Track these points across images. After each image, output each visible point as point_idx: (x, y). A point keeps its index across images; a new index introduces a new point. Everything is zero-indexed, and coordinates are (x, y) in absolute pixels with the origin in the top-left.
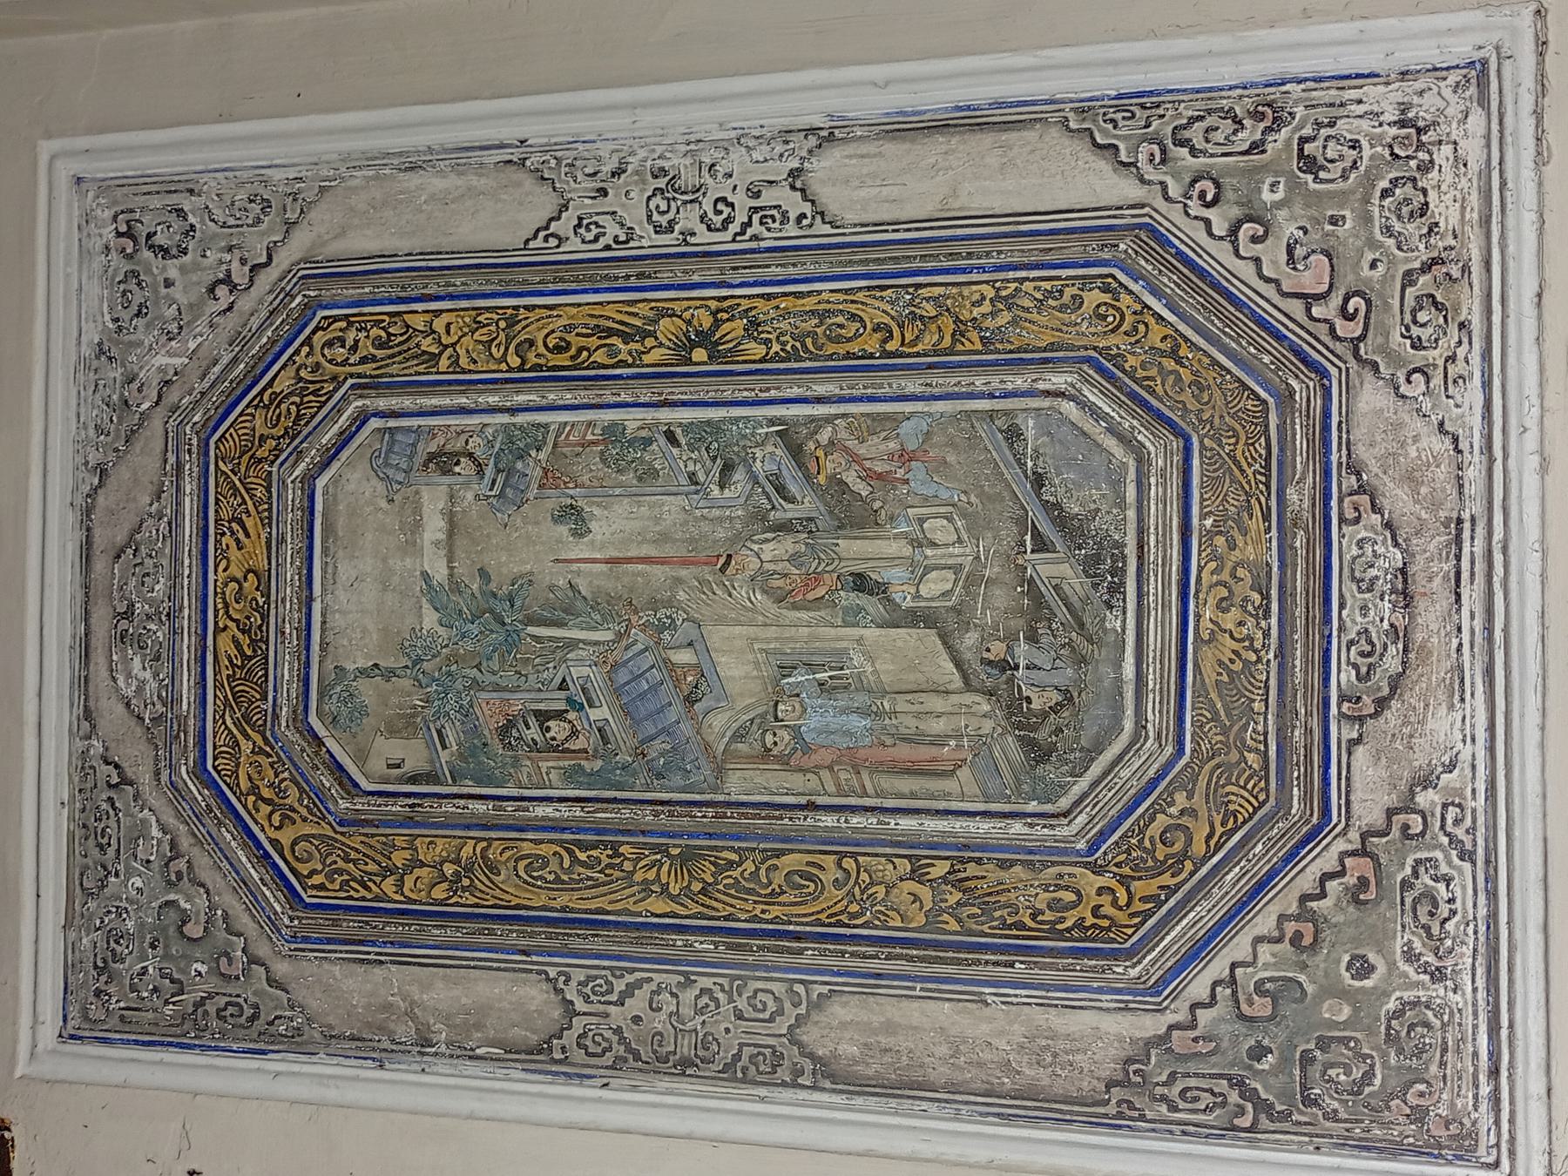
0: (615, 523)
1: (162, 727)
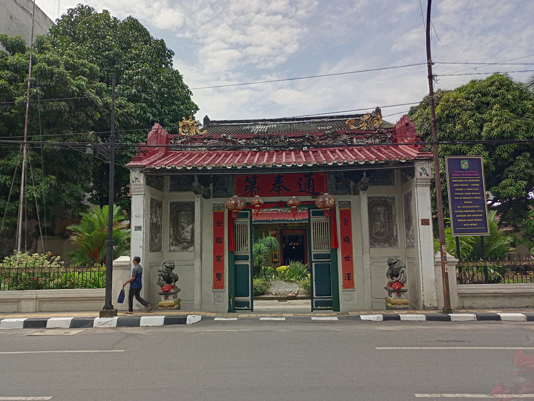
0: (383, 218)
1: (374, 201)
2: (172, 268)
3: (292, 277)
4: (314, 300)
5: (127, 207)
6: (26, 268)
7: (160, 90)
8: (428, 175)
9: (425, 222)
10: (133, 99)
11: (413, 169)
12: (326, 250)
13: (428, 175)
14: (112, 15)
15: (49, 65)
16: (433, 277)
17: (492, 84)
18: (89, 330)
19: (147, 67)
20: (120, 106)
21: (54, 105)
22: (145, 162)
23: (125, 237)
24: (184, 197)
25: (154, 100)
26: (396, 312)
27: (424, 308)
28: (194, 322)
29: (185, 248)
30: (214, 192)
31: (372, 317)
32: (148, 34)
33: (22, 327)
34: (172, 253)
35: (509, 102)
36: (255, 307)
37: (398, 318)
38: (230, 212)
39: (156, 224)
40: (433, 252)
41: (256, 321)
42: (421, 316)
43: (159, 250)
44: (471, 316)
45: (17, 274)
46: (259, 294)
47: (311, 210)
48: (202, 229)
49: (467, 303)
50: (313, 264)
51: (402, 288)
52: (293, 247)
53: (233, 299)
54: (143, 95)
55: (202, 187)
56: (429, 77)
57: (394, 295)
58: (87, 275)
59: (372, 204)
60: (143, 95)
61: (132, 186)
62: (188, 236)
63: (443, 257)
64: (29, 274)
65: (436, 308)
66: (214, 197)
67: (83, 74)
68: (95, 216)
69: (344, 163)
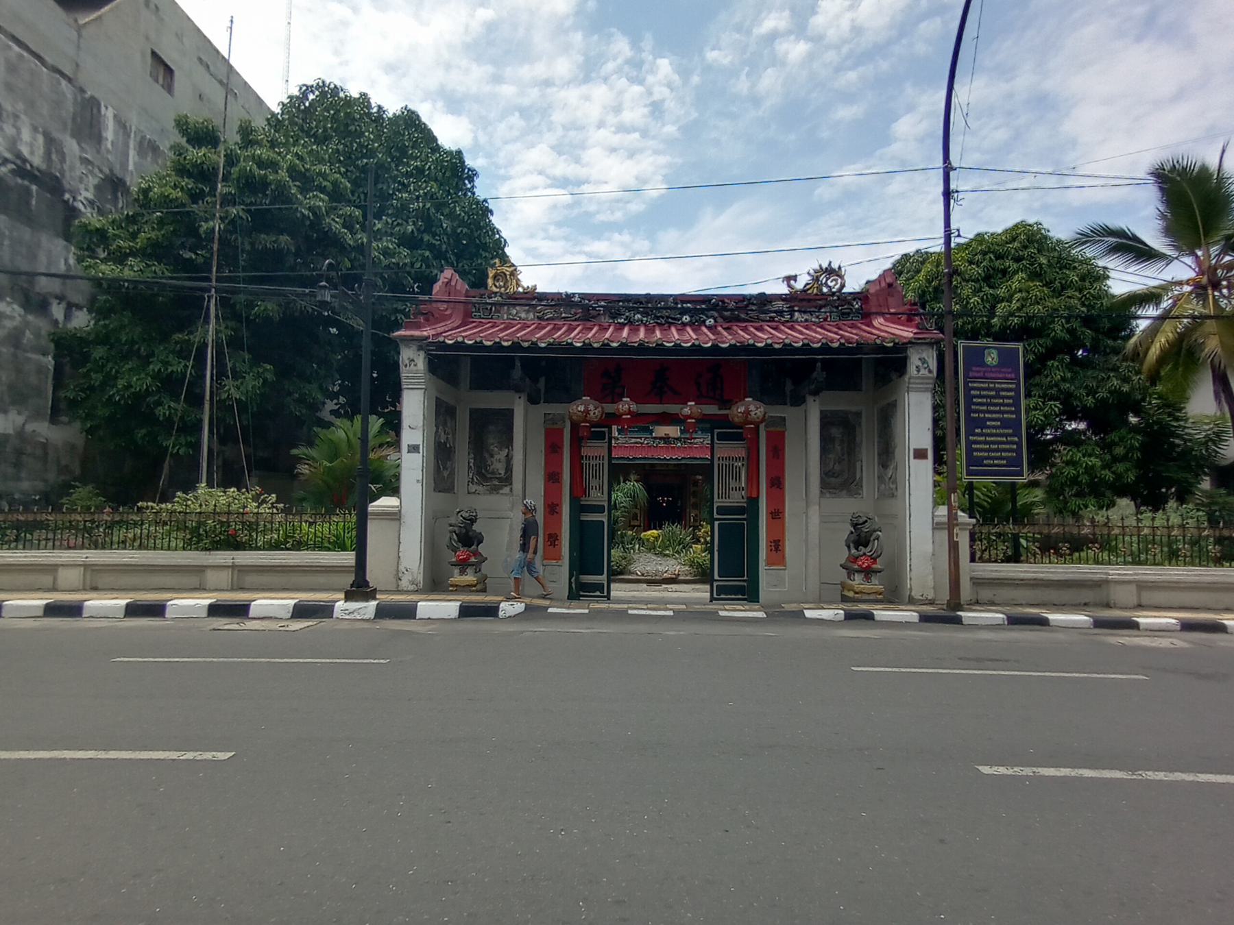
2: (473, 521)
3: (667, 548)
4: (715, 584)
5: (394, 424)
6: (215, 513)
7: (454, 229)
8: (930, 371)
9: (920, 454)
10: (411, 242)
13: (930, 371)
14: (375, 101)
15: (259, 167)
16: (929, 548)
17: (1014, 239)
18: (326, 623)
19: (433, 187)
20: (386, 253)
21: (266, 240)
22: (427, 332)
23: (392, 472)
24: (493, 400)
25: (444, 247)
26: (863, 607)
27: (912, 601)
28: (513, 614)
29: (495, 490)
31: (826, 614)
32: (435, 139)
33: (204, 614)
35: (1041, 268)
36: (613, 594)
37: (869, 617)
38: (575, 427)
39: (445, 444)
40: (931, 505)
41: (622, 615)
42: (909, 615)
44: (998, 617)
45: (199, 524)
46: (617, 574)
49: (986, 594)
50: (716, 523)
51: (874, 566)
52: (671, 497)
53: (577, 579)
54: (426, 237)
57: (858, 578)
58: (325, 529)
59: (827, 421)
60: (426, 237)
61: (405, 373)
62: (500, 468)
63: (952, 517)
64: (221, 523)
65: (931, 603)
67: (322, 190)
68: (341, 434)
69: (785, 345)
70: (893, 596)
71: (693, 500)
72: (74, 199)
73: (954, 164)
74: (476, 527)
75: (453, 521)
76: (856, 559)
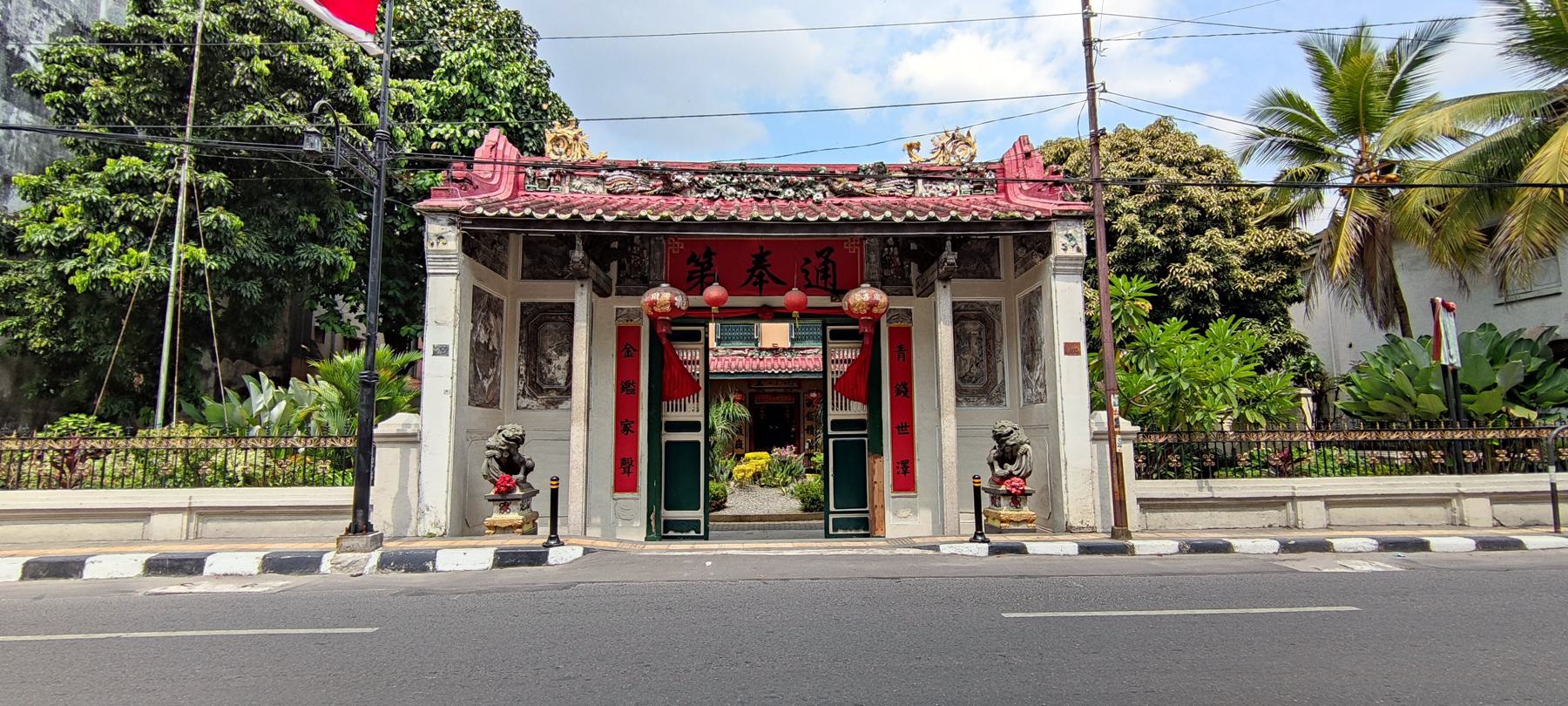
4: (831, 517)
8: (1079, 250)
9: (1071, 349)
11: (1049, 236)
12: (857, 411)
13: (1079, 250)
22: (461, 202)
24: (548, 292)
29: (553, 404)
30: (619, 283)
34: (526, 413)
37: (1019, 550)
39: (486, 345)
42: (1066, 547)
43: (493, 403)
47: (829, 328)
48: (587, 363)
49: (1156, 518)
55: (592, 264)
56: (1085, 44)
65: (1093, 531)
66: (619, 293)
70: (1053, 523)
71: (807, 423)
72: (22, 49)
73: (1094, 10)
74: (524, 451)
75: (492, 441)
76: (1003, 479)
